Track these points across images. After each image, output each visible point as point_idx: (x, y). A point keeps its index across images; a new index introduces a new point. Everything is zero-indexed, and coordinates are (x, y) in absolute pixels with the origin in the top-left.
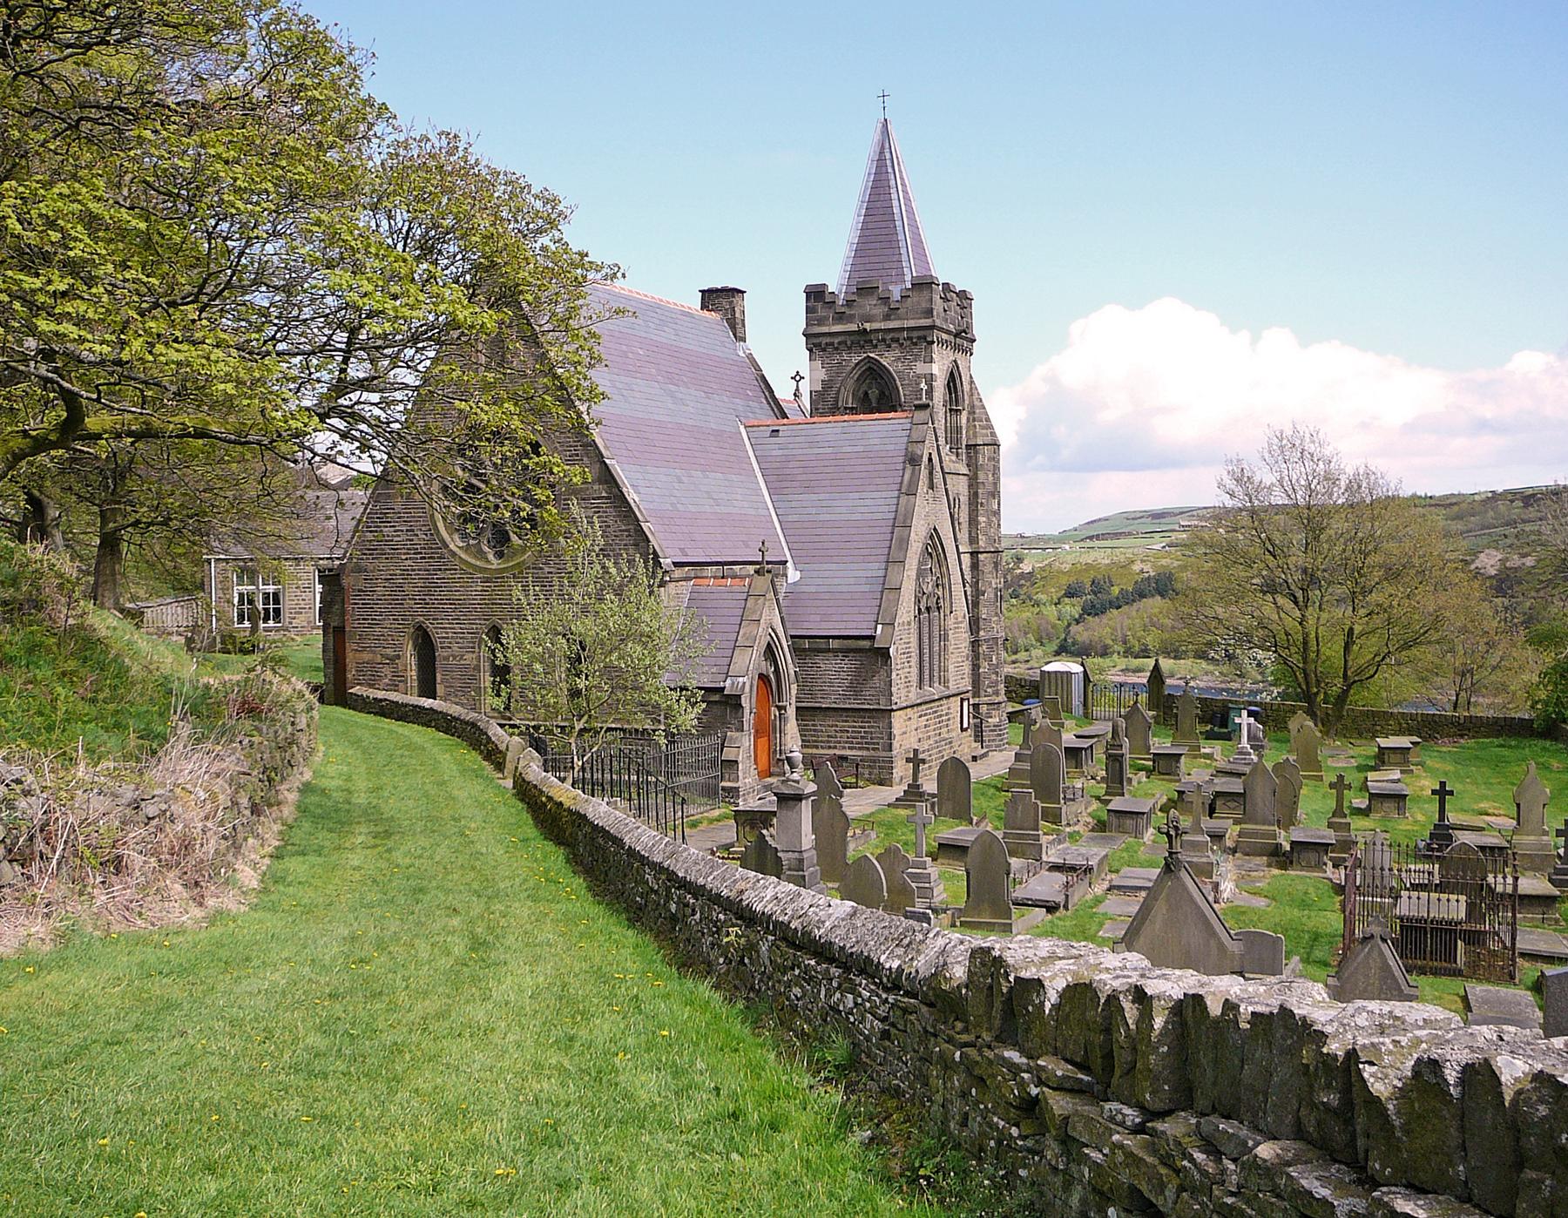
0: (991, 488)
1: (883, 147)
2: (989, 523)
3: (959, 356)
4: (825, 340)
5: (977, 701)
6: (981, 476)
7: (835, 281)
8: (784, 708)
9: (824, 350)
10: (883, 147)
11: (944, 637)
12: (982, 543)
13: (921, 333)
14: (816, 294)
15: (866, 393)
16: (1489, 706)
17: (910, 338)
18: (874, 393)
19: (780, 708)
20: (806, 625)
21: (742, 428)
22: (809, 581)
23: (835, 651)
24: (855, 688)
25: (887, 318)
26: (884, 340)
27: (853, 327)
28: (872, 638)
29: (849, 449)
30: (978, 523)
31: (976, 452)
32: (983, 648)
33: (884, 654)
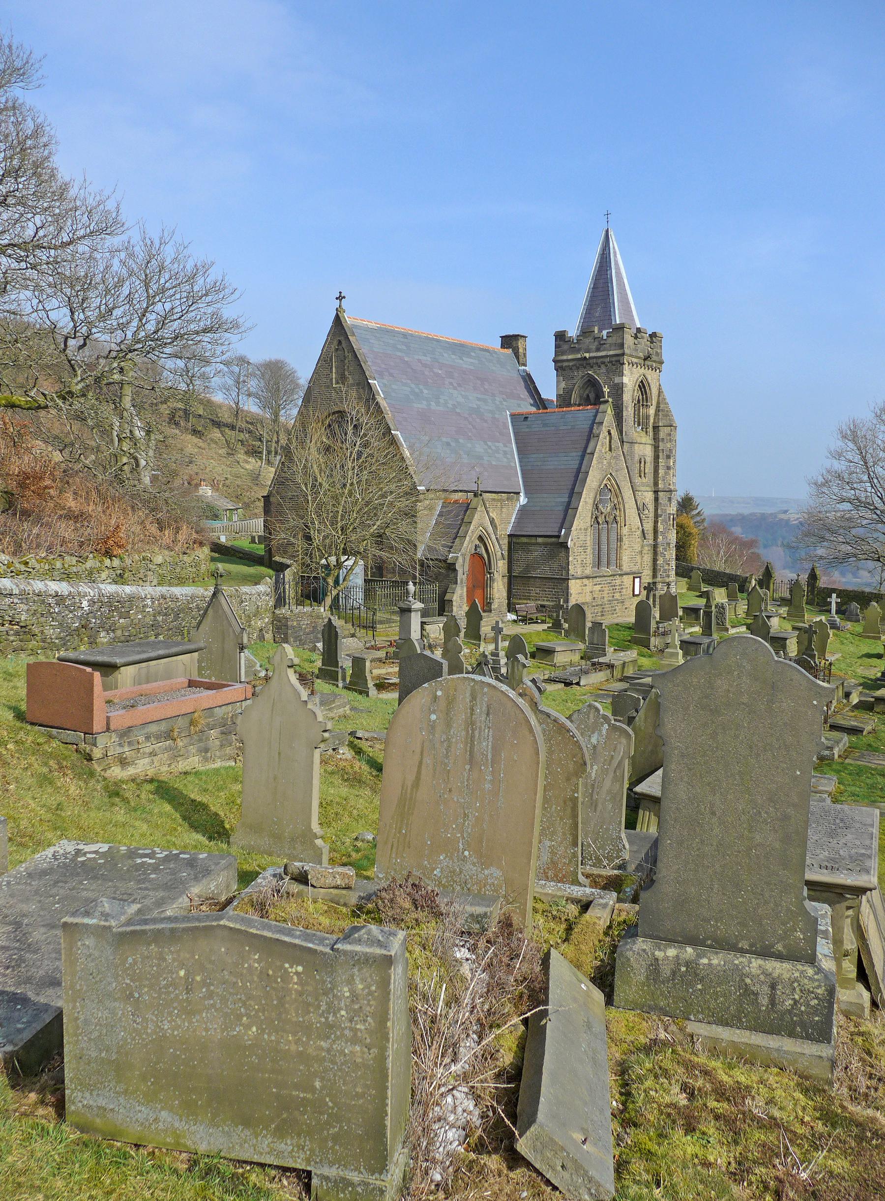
3: (651, 376)
11: (620, 539)
14: (560, 337)
15: (588, 396)
16: (462, 580)
18: (592, 396)
20: (526, 529)
25: (598, 350)
27: (579, 356)
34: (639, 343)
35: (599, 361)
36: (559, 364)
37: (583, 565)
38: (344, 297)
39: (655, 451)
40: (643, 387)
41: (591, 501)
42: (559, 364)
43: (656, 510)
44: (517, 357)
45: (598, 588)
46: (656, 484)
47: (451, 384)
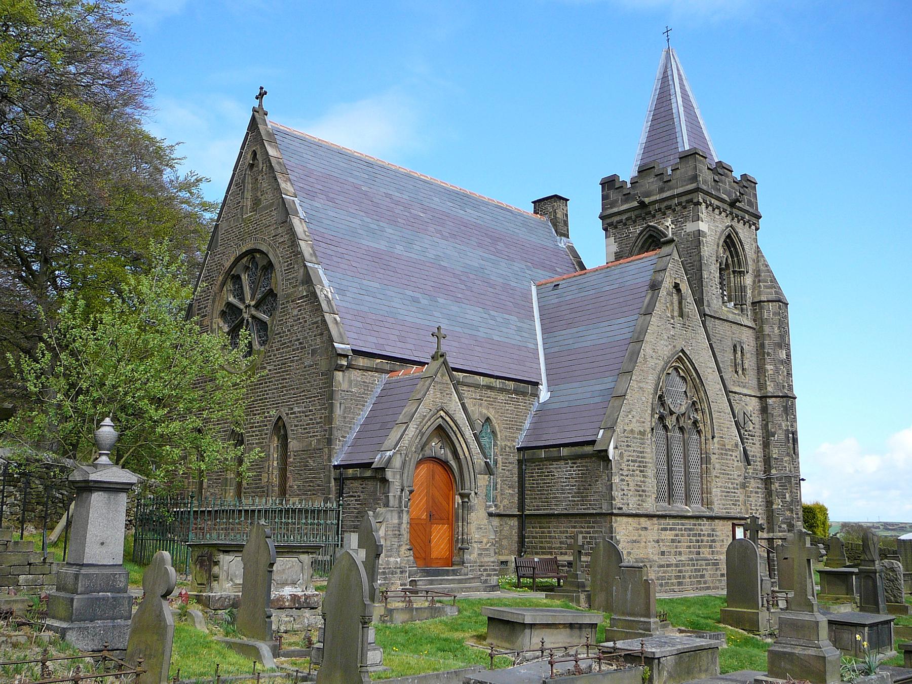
0: (777, 340)
1: (666, 67)
2: (777, 371)
3: (740, 228)
4: (617, 218)
5: (771, 535)
6: (767, 329)
7: (627, 173)
8: (468, 496)
9: (616, 227)
10: (666, 67)
11: (705, 460)
12: (770, 389)
13: (689, 197)
14: (609, 184)
17: (680, 204)
19: (462, 496)
21: (534, 289)
22: (556, 399)
23: (564, 459)
24: (582, 493)
25: (662, 190)
26: (660, 209)
28: (593, 443)
29: (607, 288)
30: (765, 371)
31: (761, 308)
32: (776, 486)
33: (602, 456)
34: (721, 181)
35: (663, 206)
36: (609, 221)
37: (641, 492)
38: (266, 93)
39: (757, 338)
40: (730, 243)
41: (650, 387)
42: (609, 221)
43: (765, 427)
44: (555, 225)
45: (669, 535)
46: (761, 386)
47: (439, 232)
